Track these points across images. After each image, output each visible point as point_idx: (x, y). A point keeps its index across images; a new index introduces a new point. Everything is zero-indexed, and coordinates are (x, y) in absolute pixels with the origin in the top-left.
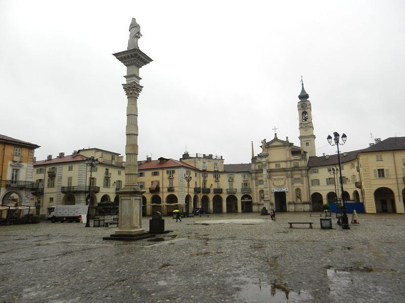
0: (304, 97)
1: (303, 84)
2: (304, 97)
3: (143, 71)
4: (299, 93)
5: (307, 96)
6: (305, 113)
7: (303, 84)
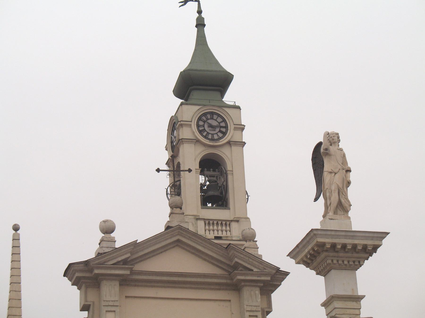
0: (203, 83)
1: (200, 24)
2: (203, 83)
3: (368, 276)
4: (182, 59)
5: (220, 81)
6: (211, 165)
7: (200, 24)
